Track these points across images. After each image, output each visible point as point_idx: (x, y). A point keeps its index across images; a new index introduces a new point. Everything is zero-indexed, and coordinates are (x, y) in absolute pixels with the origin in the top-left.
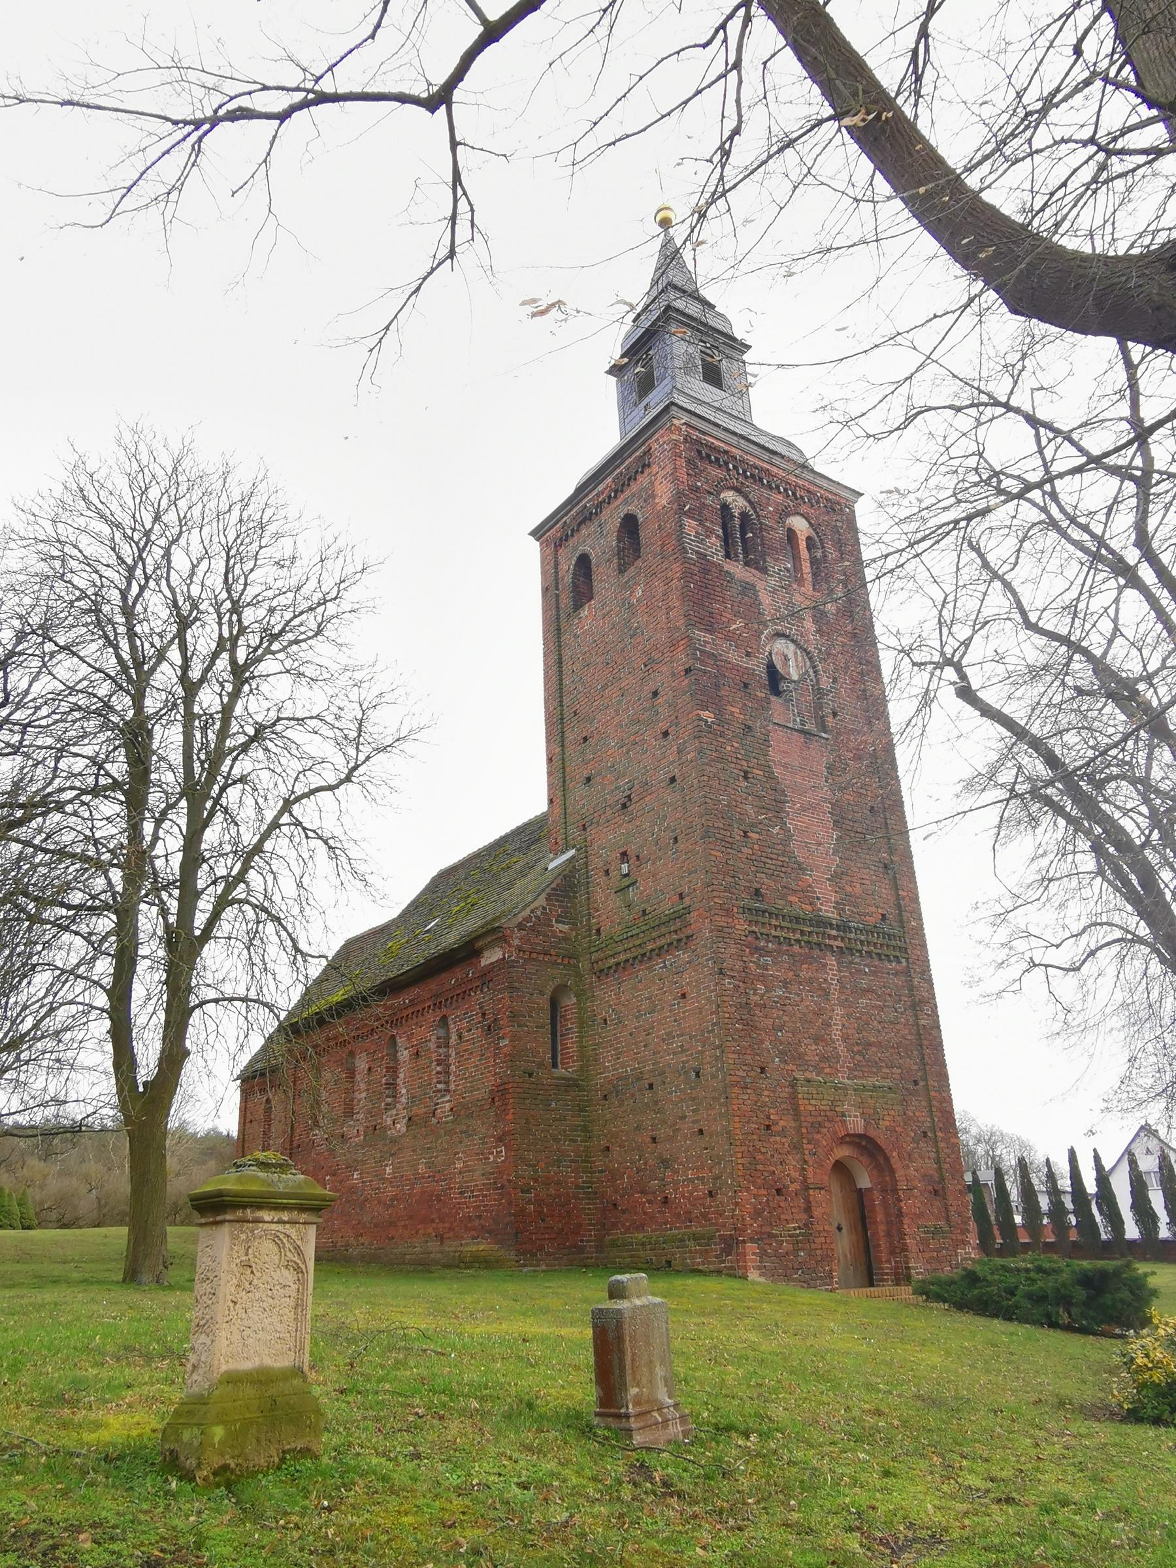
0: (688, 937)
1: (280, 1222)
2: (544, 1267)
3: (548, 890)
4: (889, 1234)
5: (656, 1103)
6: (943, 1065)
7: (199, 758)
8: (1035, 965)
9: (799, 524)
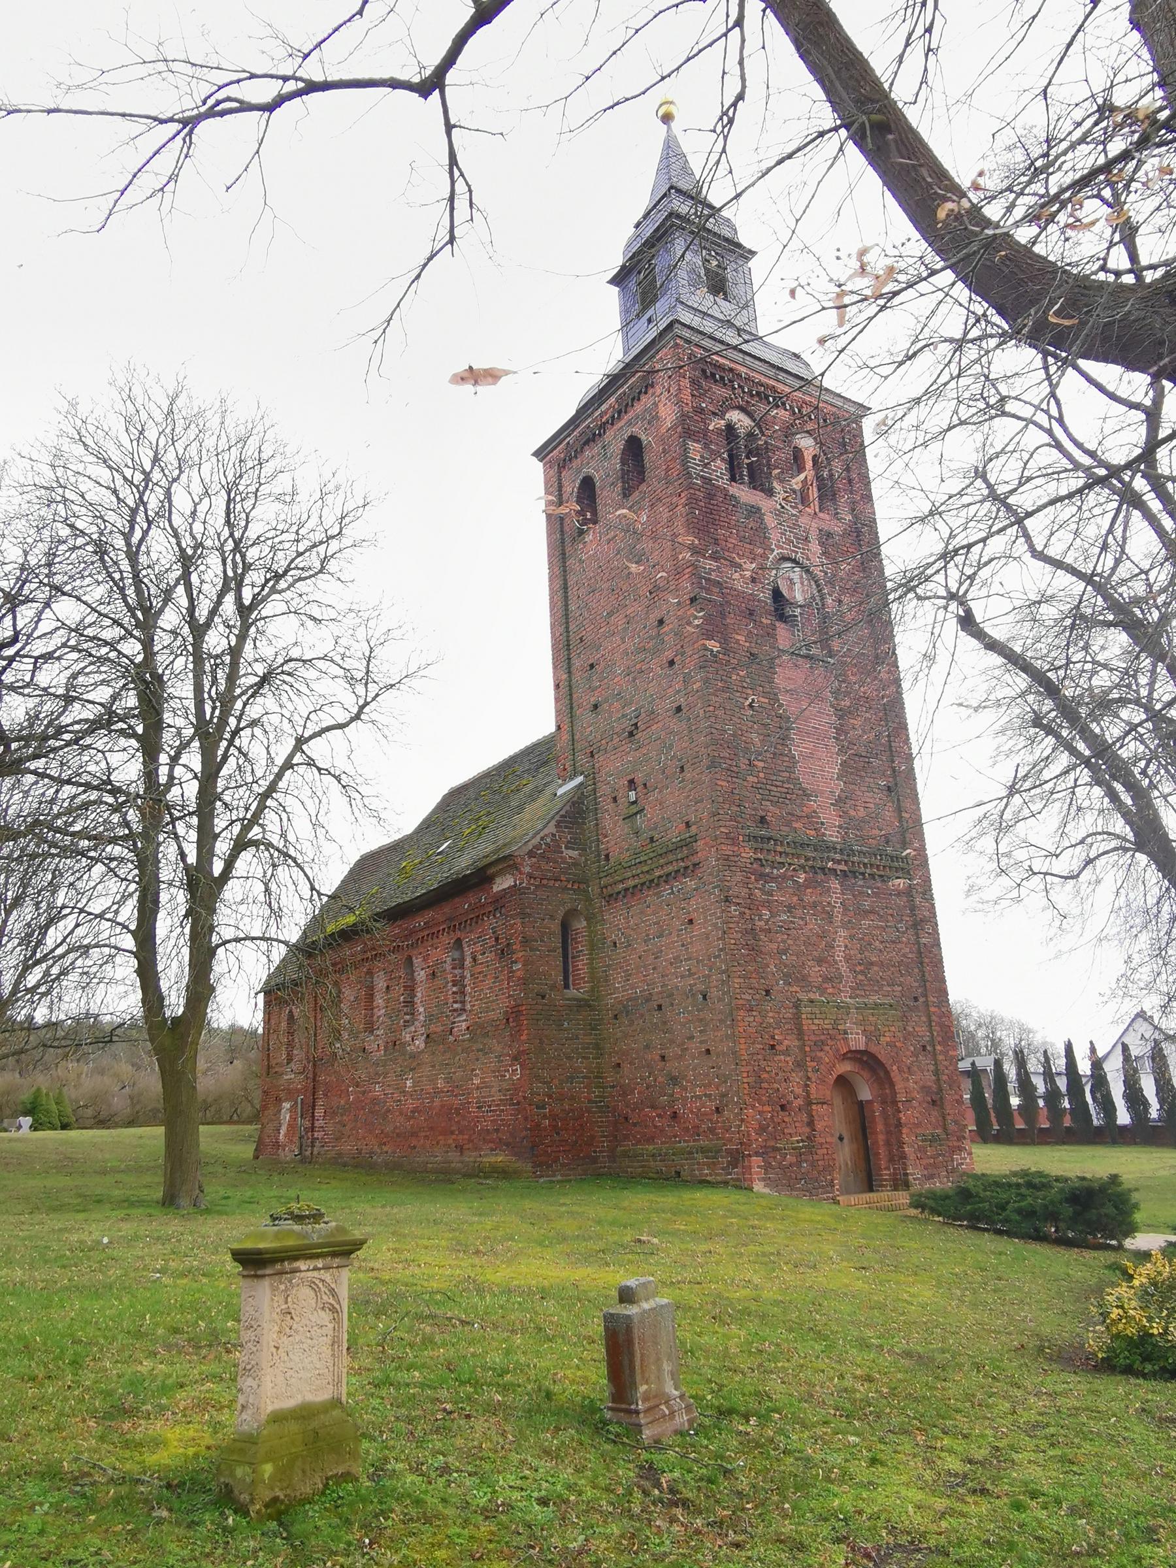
0: (695, 865)
1: (316, 1269)
2: (559, 1178)
3: (557, 818)
4: (888, 1143)
5: (665, 1023)
6: (943, 981)
7: (210, 697)
8: (1035, 874)
9: (806, 443)
